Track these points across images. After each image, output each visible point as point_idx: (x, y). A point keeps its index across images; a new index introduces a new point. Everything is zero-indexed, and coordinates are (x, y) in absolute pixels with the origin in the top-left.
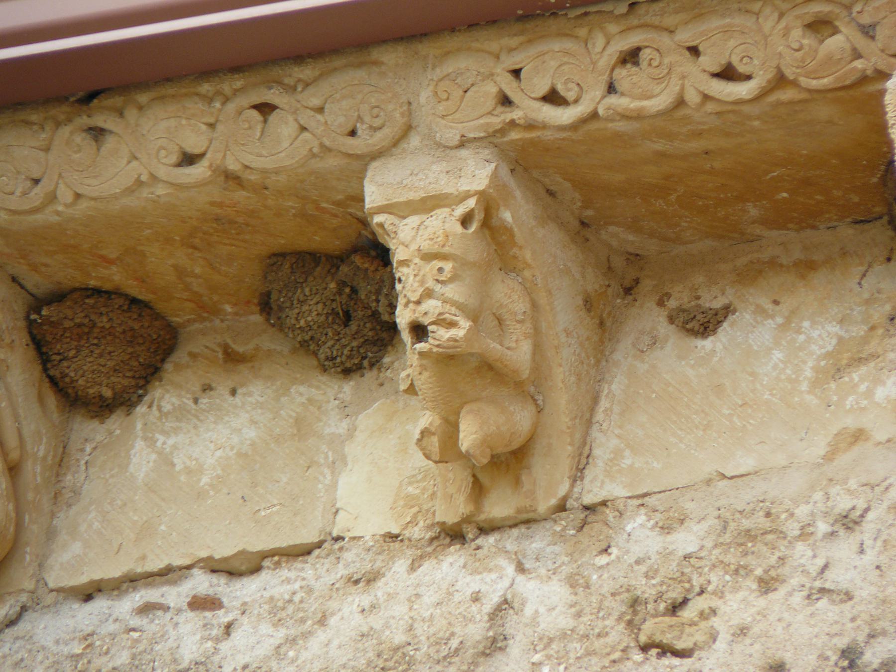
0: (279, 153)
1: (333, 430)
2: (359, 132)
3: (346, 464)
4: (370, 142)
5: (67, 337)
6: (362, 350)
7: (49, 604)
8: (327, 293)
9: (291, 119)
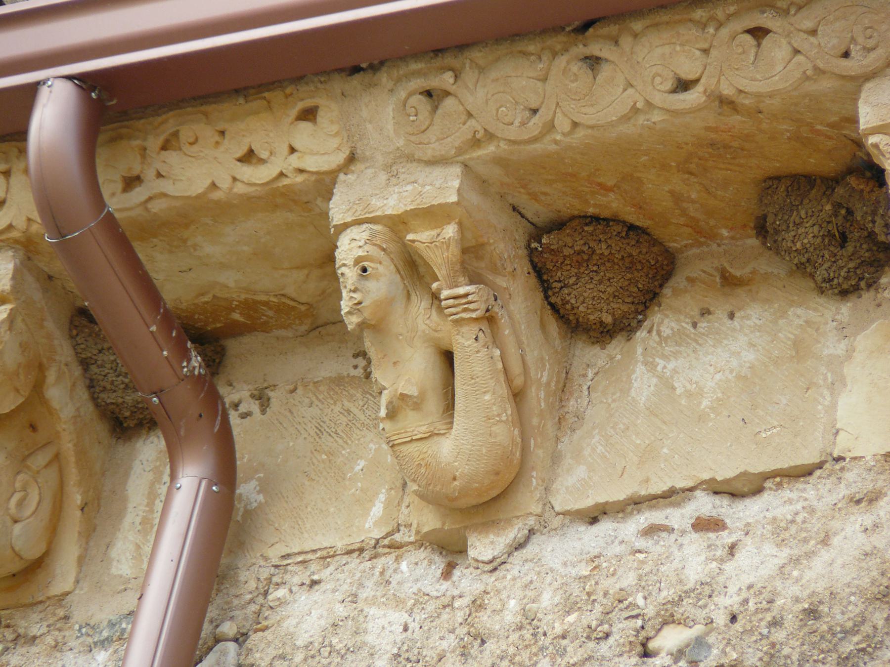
0: (773, 76)
1: (831, 351)
2: (853, 54)
3: (845, 385)
4: (864, 63)
5: (567, 265)
6: (858, 272)
8: (823, 215)
9: (784, 42)
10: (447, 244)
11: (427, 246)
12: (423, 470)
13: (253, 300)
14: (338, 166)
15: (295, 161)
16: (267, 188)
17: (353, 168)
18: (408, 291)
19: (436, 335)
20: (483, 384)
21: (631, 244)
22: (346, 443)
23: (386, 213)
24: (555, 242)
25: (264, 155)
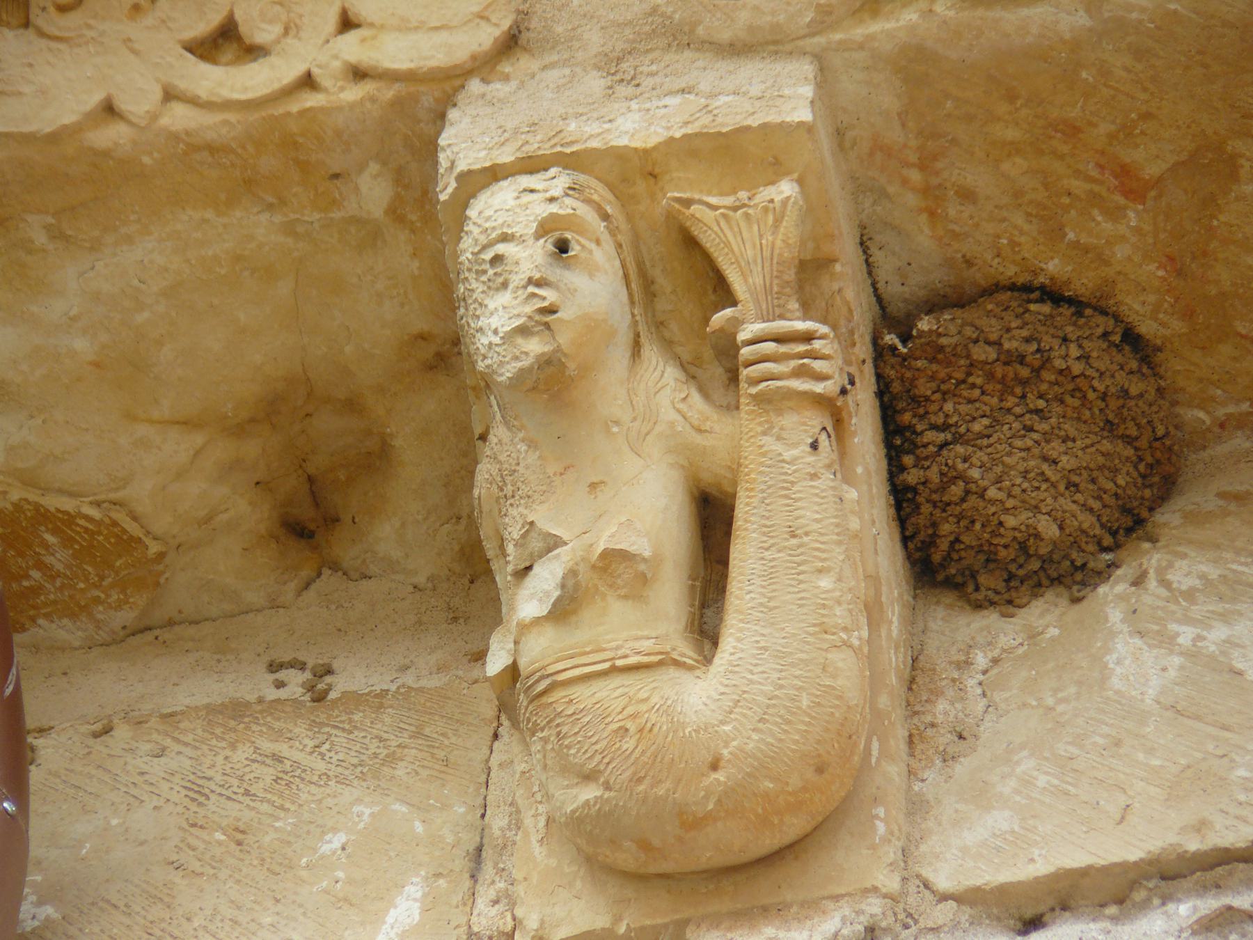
5: (973, 386)
7: (940, 922)
10: (777, 213)
11: (723, 215)
12: (629, 744)
13: (37, 507)
14: (474, 58)
15: (351, 48)
16: (254, 117)
17: (506, 67)
18: (637, 335)
19: (699, 439)
20: (817, 549)
21: (1127, 368)
22: (282, 808)
23: (614, 143)
24: (953, 329)
25: (263, 34)
